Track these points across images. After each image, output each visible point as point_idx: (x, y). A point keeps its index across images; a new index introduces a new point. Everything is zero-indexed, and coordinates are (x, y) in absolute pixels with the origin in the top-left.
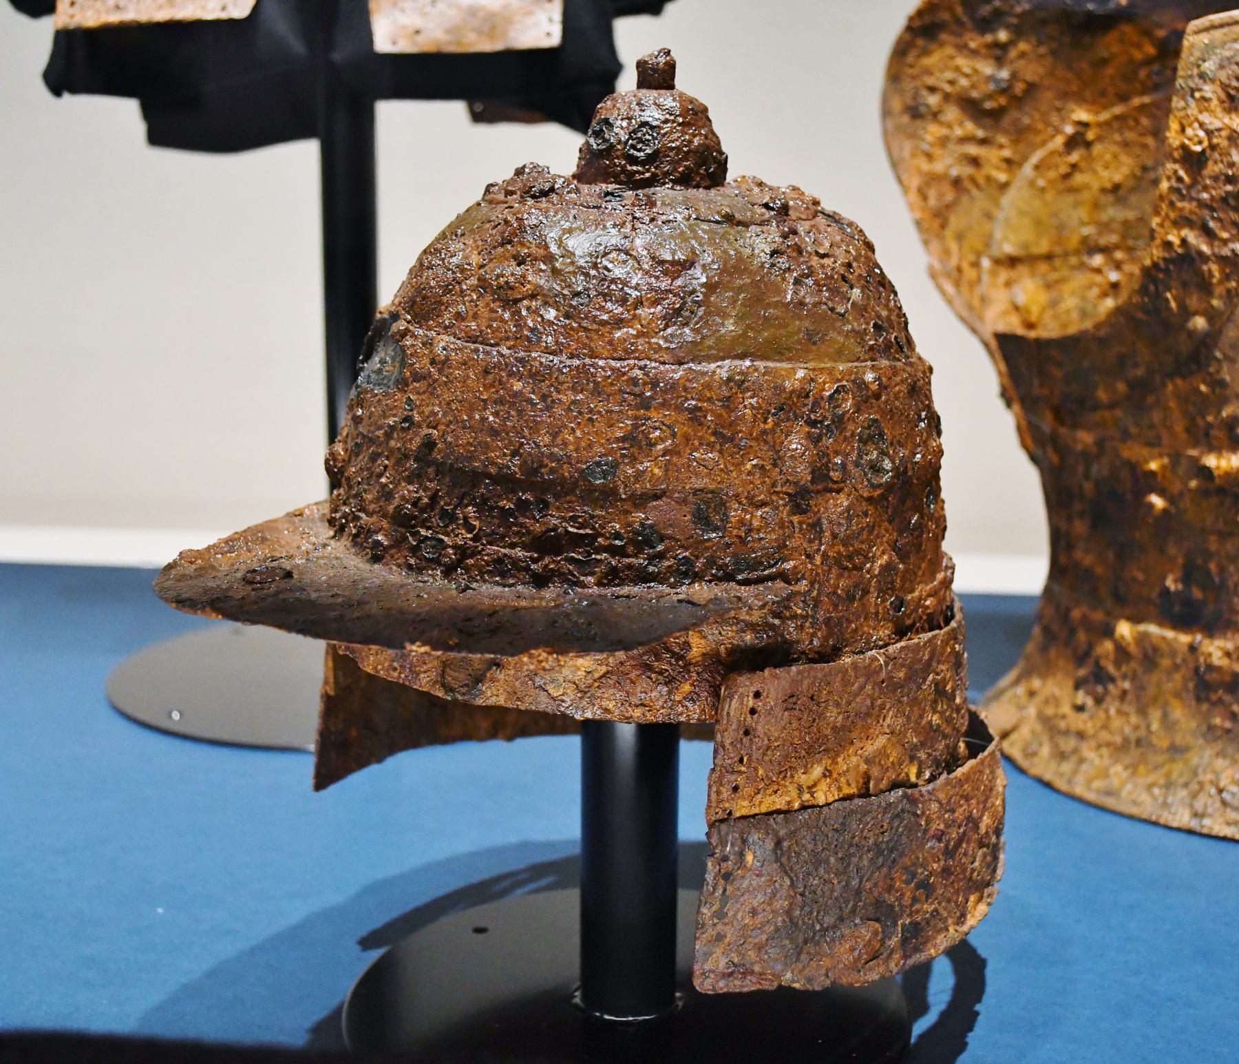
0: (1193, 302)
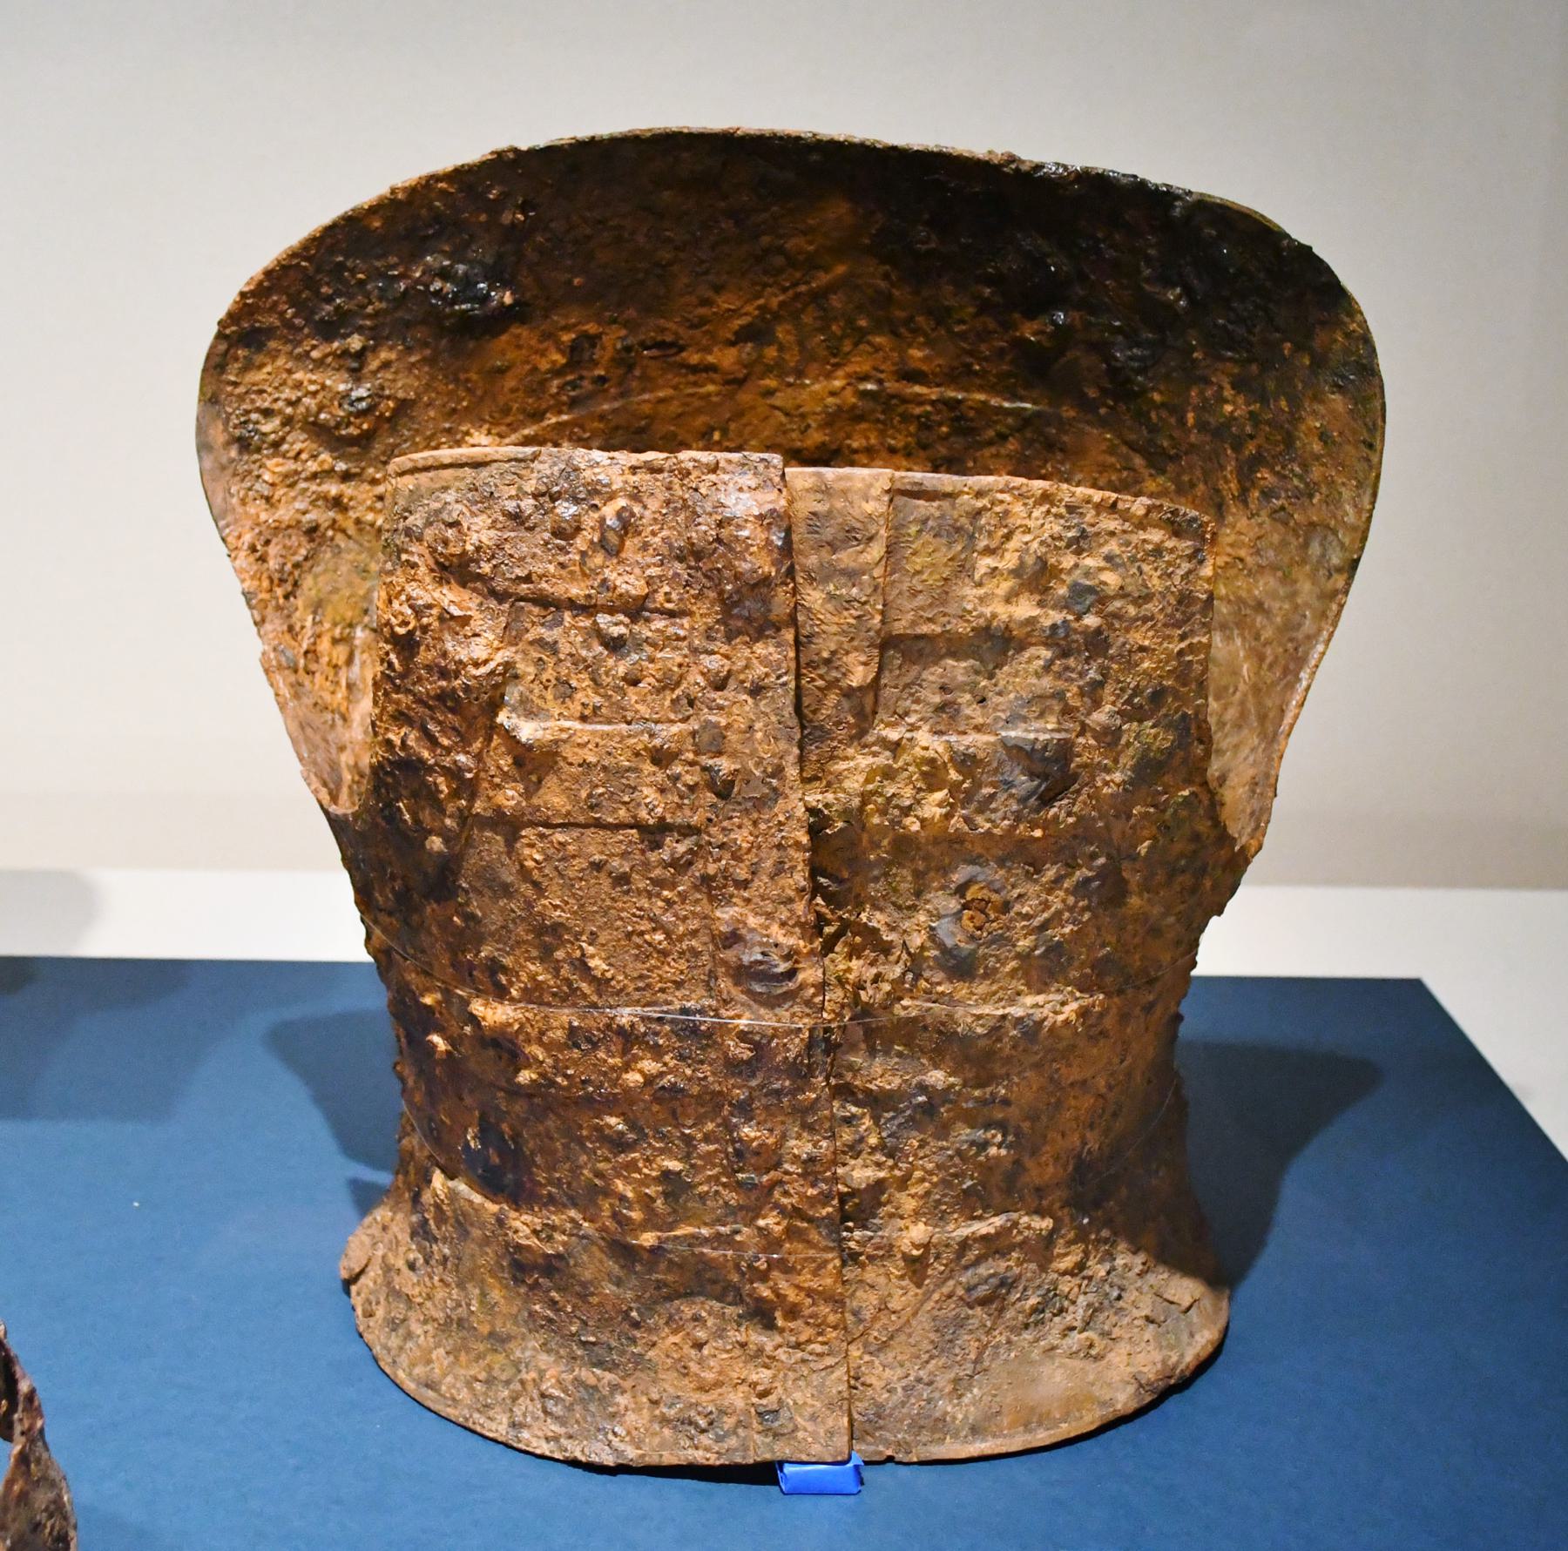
0: (426, 816)
